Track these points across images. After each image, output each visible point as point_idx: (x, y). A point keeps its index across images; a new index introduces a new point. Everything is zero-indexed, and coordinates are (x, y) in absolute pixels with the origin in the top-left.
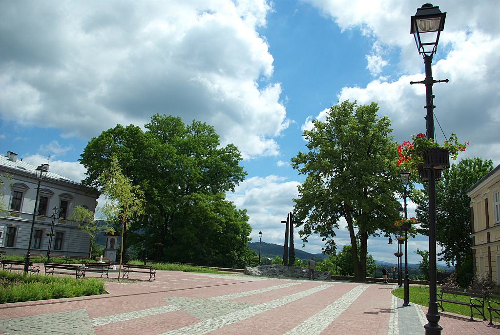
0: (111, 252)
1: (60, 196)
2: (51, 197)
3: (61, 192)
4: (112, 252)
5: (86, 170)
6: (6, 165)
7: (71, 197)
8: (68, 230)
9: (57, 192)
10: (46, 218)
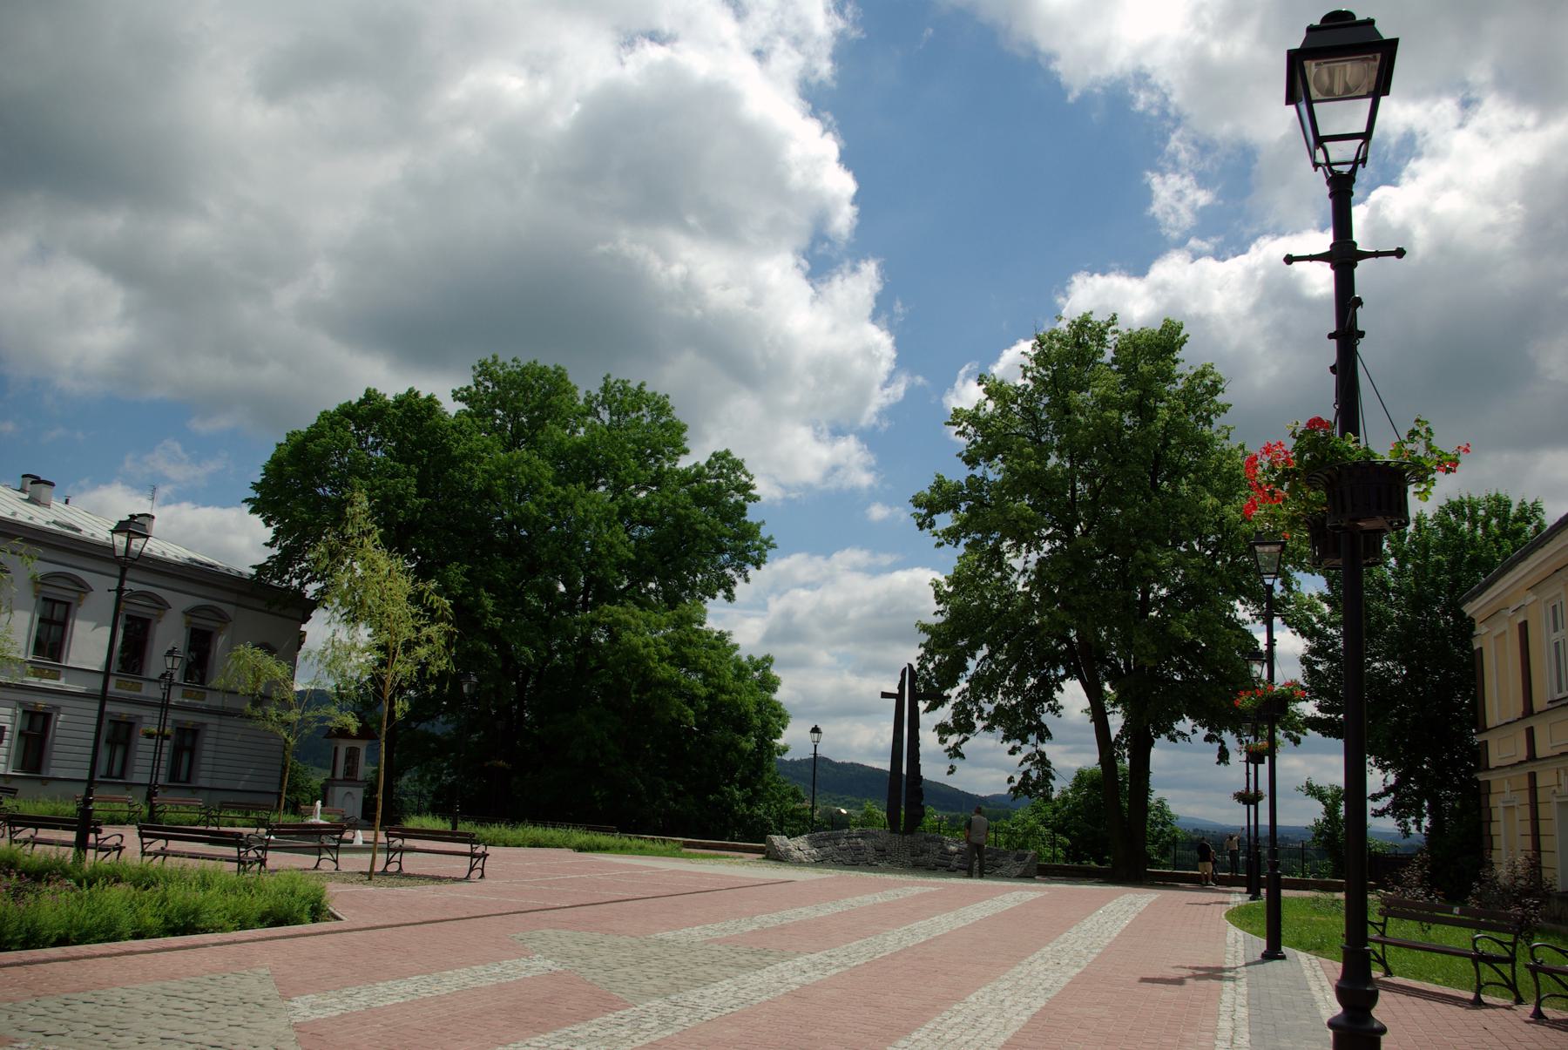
0: (347, 789)
1: (191, 613)
2: (160, 616)
3: (190, 602)
4: (350, 789)
5: (268, 533)
6: (168, 556)
7: (223, 618)
8: (211, 720)
9: (180, 602)
10: (63, 671)
